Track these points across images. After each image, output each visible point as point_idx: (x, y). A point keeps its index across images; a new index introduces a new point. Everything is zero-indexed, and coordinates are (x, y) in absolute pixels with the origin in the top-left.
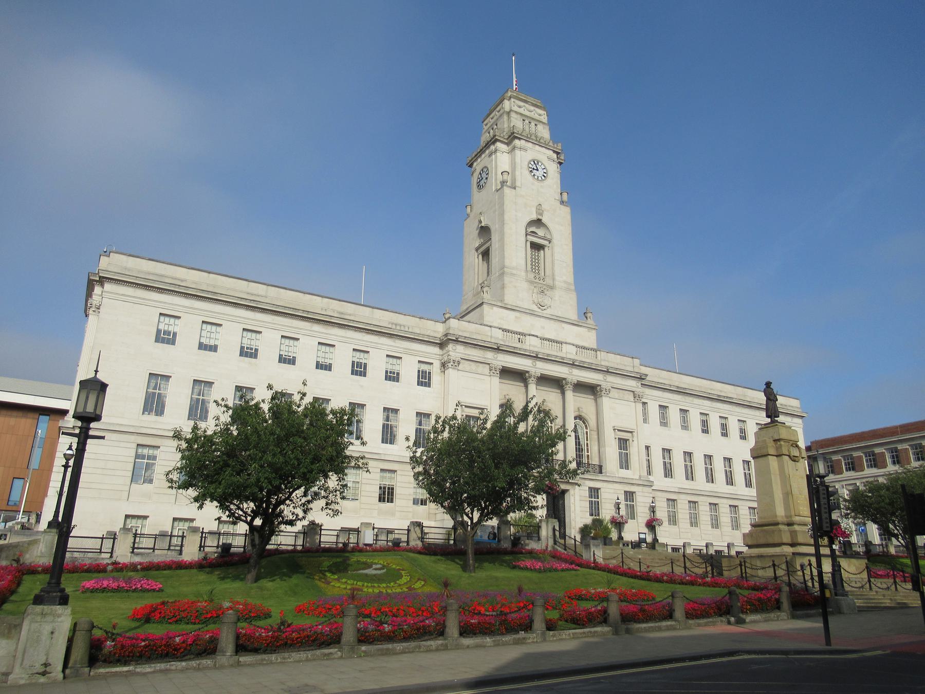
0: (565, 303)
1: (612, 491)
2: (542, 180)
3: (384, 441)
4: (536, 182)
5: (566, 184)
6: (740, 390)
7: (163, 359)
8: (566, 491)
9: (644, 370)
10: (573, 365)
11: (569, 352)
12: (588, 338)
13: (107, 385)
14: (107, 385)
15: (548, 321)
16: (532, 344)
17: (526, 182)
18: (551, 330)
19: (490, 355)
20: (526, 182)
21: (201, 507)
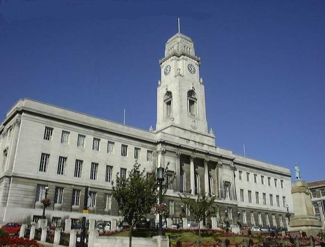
0: (202, 126)
12: (211, 142)
17: (178, 72)
20: (178, 72)
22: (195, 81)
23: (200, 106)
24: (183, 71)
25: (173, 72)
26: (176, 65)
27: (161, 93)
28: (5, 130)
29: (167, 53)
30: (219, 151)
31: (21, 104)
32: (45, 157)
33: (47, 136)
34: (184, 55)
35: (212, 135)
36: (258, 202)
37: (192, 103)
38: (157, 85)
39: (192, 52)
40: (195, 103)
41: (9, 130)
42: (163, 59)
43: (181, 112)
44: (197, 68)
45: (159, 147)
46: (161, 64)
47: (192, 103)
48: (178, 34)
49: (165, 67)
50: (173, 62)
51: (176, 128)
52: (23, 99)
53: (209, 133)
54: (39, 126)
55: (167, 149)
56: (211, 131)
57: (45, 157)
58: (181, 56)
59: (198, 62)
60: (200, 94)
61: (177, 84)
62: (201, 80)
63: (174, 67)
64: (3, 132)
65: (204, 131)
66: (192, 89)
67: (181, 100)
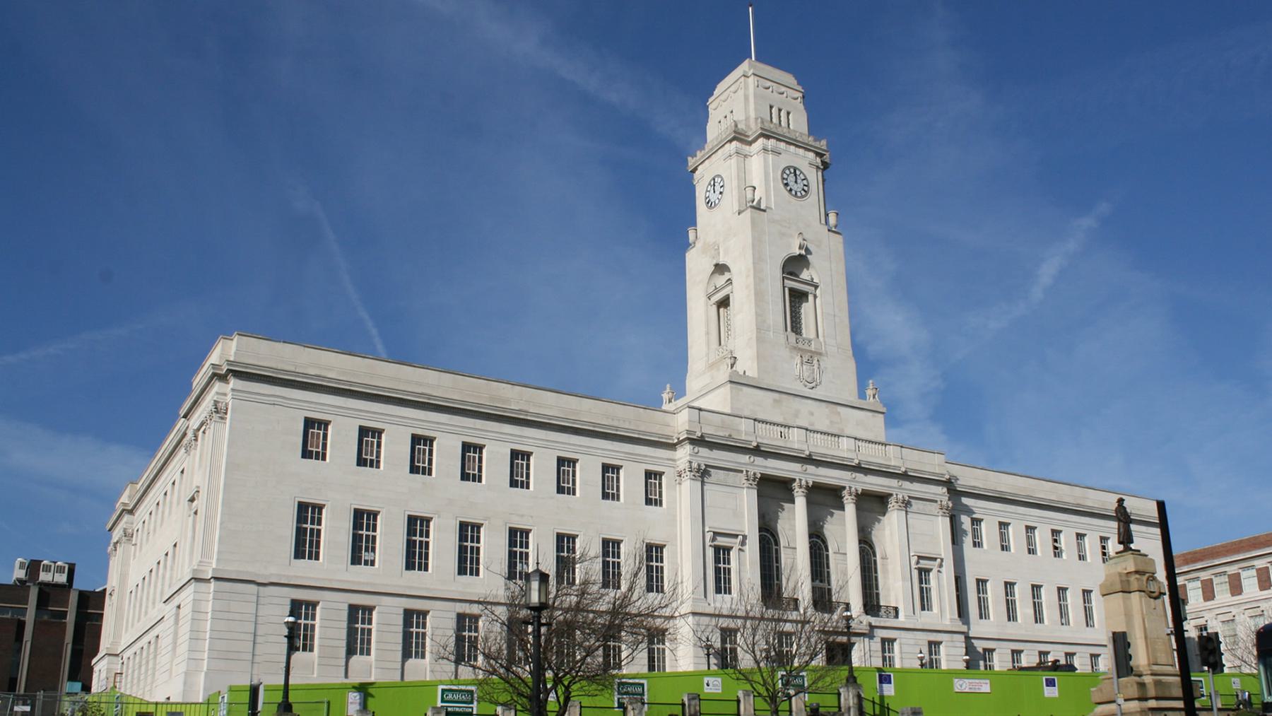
0: (840, 376)
1: (912, 642)
2: (802, 197)
3: (410, 566)
4: (793, 200)
5: (829, 200)
6: (1078, 491)
7: (312, 480)
8: (991, 651)
9: (955, 470)
10: (858, 468)
11: (844, 449)
12: (875, 426)
13: (1114, 633)
14: (1114, 633)
15: (818, 403)
16: (795, 441)
17: (748, 170)
18: (821, 417)
19: (745, 458)
20: (748, 170)
21: (372, 696)
22: (807, 222)
23: (827, 314)
24: (767, 191)
25: (730, 201)
26: (743, 173)
27: (697, 264)
28: (190, 434)
29: (715, 129)
30: (893, 457)
31: (224, 351)
32: (308, 513)
33: (312, 447)
34: (768, 137)
35: (871, 402)
36: (1038, 618)
37: (797, 297)
38: (686, 245)
39: (798, 123)
40: (811, 298)
41: (200, 432)
42: (699, 154)
43: (761, 328)
44: (814, 177)
45: (684, 454)
46: (696, 169)
47: (797, 297)
48: (745, 66)
49: (708, 178)
50: (734, 161)
51: (745, 389)
52: (228, 335)
53: (862, 395)
54: (286, 414)
55: (711, 463)
56: (869, 392)
57: (308, 513)
58: (755, 140)
59: (820, 155)
60: (827, 271)
61: (746, 236)
62: (832, 219)
63: (735, 183)
64: (185, 441)
65: (850, 395)
66: (797, 252)
67: (759, 296)
